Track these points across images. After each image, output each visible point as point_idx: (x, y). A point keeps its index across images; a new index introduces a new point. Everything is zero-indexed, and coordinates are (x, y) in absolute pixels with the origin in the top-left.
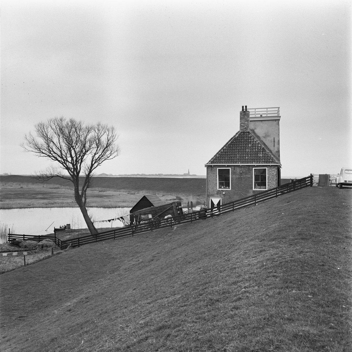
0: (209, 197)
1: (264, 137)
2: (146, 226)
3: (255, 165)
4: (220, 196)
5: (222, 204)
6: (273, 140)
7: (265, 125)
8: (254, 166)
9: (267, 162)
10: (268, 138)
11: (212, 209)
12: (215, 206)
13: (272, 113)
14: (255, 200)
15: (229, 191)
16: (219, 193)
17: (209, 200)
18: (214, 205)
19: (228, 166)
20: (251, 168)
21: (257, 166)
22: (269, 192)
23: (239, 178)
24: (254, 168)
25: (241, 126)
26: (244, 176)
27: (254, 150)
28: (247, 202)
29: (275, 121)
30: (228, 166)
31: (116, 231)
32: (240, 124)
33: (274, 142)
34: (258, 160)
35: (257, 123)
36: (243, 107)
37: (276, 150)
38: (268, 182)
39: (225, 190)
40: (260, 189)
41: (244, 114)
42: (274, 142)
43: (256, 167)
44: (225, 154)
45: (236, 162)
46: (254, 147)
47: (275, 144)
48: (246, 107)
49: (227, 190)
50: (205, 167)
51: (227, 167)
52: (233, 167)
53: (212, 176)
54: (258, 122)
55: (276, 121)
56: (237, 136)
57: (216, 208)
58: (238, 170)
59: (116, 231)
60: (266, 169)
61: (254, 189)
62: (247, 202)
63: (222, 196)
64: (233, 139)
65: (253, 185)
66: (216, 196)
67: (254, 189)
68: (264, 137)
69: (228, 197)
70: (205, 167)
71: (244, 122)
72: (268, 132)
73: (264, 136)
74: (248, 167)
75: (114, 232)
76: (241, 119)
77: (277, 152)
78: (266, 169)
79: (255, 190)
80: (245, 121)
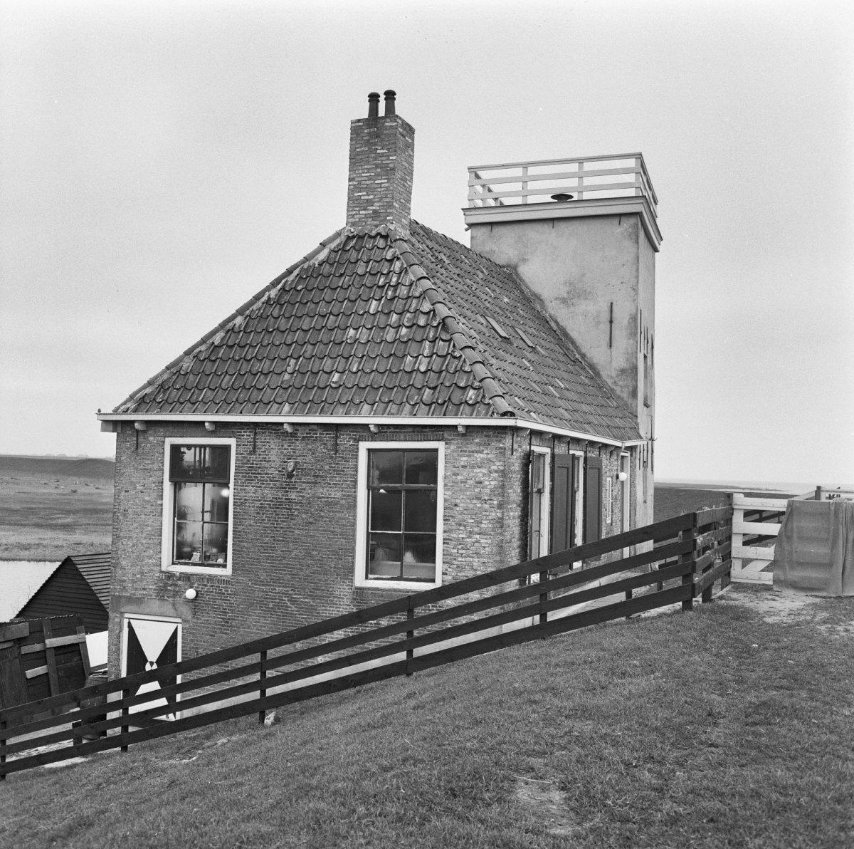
0: (122, 617)
1: (564, 301)
2: (638, 582)
3: (455, 427)
4: (172, 612)
5: (182, 657)
6: (605, 317)
7: (566, 241)
8: (362, 431)
9: (443, 406)
10: (583, 306)
11: (128, 687)
12: (148, 667)
13: (616, 185)
14: (408, 646)
15: (351, 570)
16: (168, 586)
17: (121, 630)
18: (146, 661)
19: (221, 428)
20: (345, 440)
21: (385, 431)
22: (450, 603)
23: (277, 505)
24: (364, 446)
25: (354, 203)
26: (308, 493)
27: (390, 335)
28: (321, 659)
29: (616, 221)
30: (221, 428)
31: (272, 653)
32: (351, 192)
33: (611, 322)
34: (395, 388)
35: (532, 232)
36: (374, 98)
37: (620, 362)
38: (445, 541)
39: (200, 577)
40: (400, 578)
41: (369, 134)
42: (611, 322)
43: (373, 437)
44: (229, 361)
45: (264, 405)
46: (395, 317)
47: (616, 333)
48: (390, 95)
49: (210, 578)
50: (103, 430)
51: (212, 434)
52: (247, 435)
53: (139, 487)
54: (538, 227)
55: (623, 219)
56: (322, 256)
57: (150, 677)
58: (274, 453)
59: (272, 653)
60: (436, 450)
61: (360, 580)
62: (321, 659)
63: (186, 611)
64: (296, 272)
65: (353, 550)
66: (155, 605)
67: (360, 580)
68: (564, 301)
69: (213, 617)
70: (103, 430)
71: (370, 178)
72: (583, 275)
73: (565, 296)
74: (328, 437)
75: (255, 658)
76: (355, 160)
77: (623, 371)
78: (436, 450)
79: (372, 584)
80: (377, 175)
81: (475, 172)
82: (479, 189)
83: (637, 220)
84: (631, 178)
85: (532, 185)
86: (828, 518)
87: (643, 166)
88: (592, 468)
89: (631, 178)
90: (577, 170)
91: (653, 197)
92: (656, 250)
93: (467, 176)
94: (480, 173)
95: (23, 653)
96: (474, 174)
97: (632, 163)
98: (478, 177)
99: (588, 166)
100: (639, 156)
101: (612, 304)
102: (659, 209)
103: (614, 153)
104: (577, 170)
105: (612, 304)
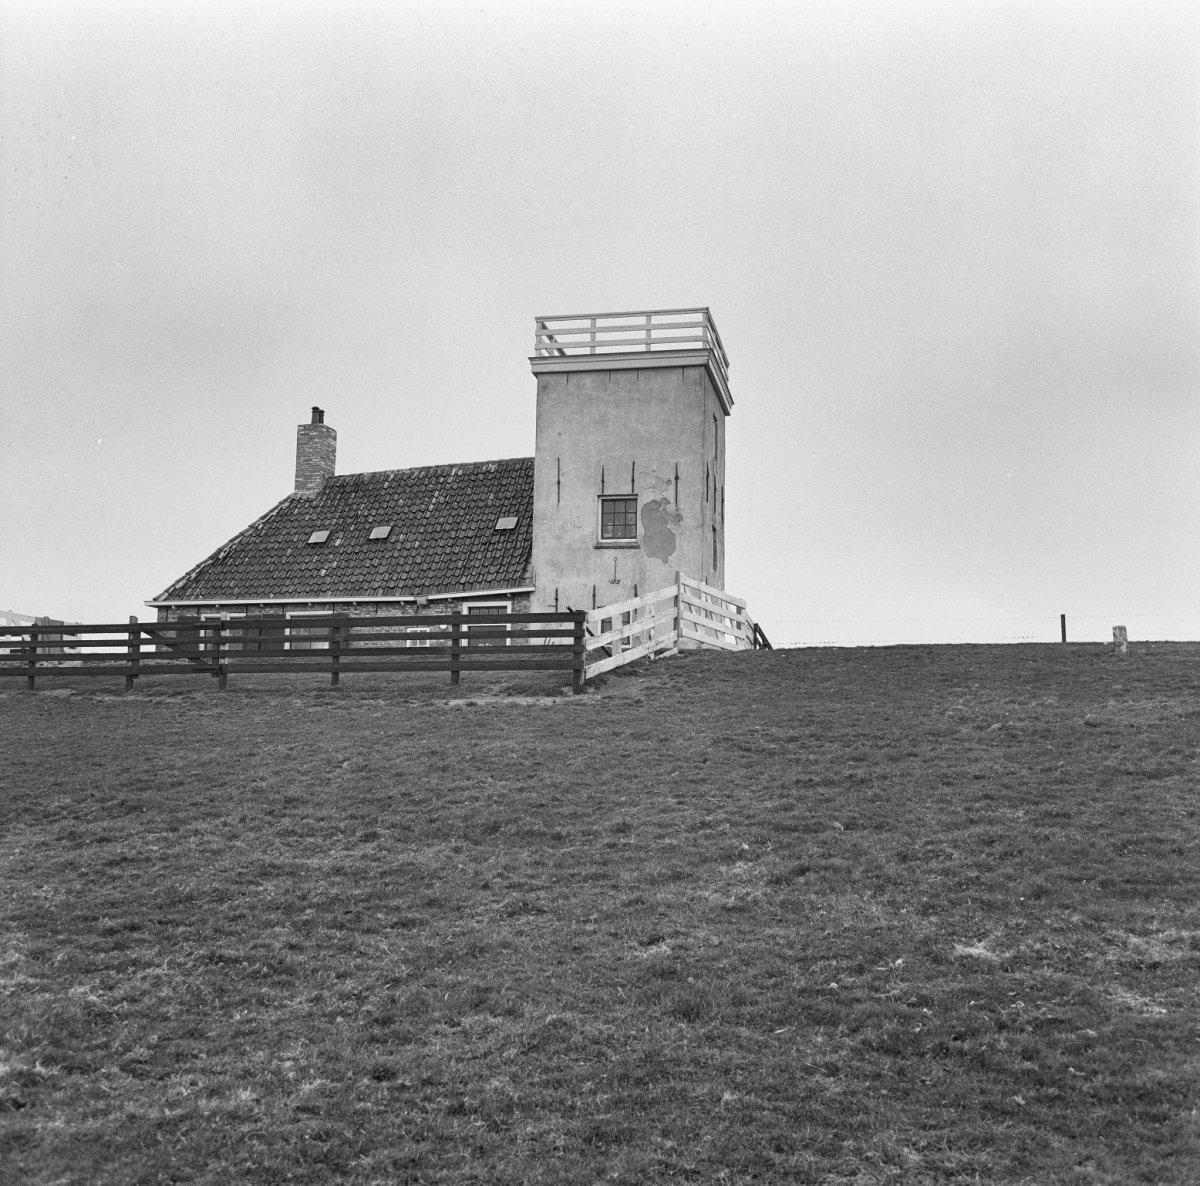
81: (542, 323)
82: (546, 340)
83: (704, 379)
84: (699, 332)
85: (600, 337)
86: (834, 695)
87: (709, 320)
88: (616, 559)
89: (699, 332)
90: (589, 326)
91: (724, 357)
92: (727, 413)
93: (534, 326)
94: (547, 324)
95: (371, 537)
96: (540, 324)
97: (699, 317)
98: (544, 327)
99: (655, 320)
100: (706, 311)
101: (1063, 617)
102: (730, 372)
103: (631, 310)
104: (589, 326)
105: (1063, 617)
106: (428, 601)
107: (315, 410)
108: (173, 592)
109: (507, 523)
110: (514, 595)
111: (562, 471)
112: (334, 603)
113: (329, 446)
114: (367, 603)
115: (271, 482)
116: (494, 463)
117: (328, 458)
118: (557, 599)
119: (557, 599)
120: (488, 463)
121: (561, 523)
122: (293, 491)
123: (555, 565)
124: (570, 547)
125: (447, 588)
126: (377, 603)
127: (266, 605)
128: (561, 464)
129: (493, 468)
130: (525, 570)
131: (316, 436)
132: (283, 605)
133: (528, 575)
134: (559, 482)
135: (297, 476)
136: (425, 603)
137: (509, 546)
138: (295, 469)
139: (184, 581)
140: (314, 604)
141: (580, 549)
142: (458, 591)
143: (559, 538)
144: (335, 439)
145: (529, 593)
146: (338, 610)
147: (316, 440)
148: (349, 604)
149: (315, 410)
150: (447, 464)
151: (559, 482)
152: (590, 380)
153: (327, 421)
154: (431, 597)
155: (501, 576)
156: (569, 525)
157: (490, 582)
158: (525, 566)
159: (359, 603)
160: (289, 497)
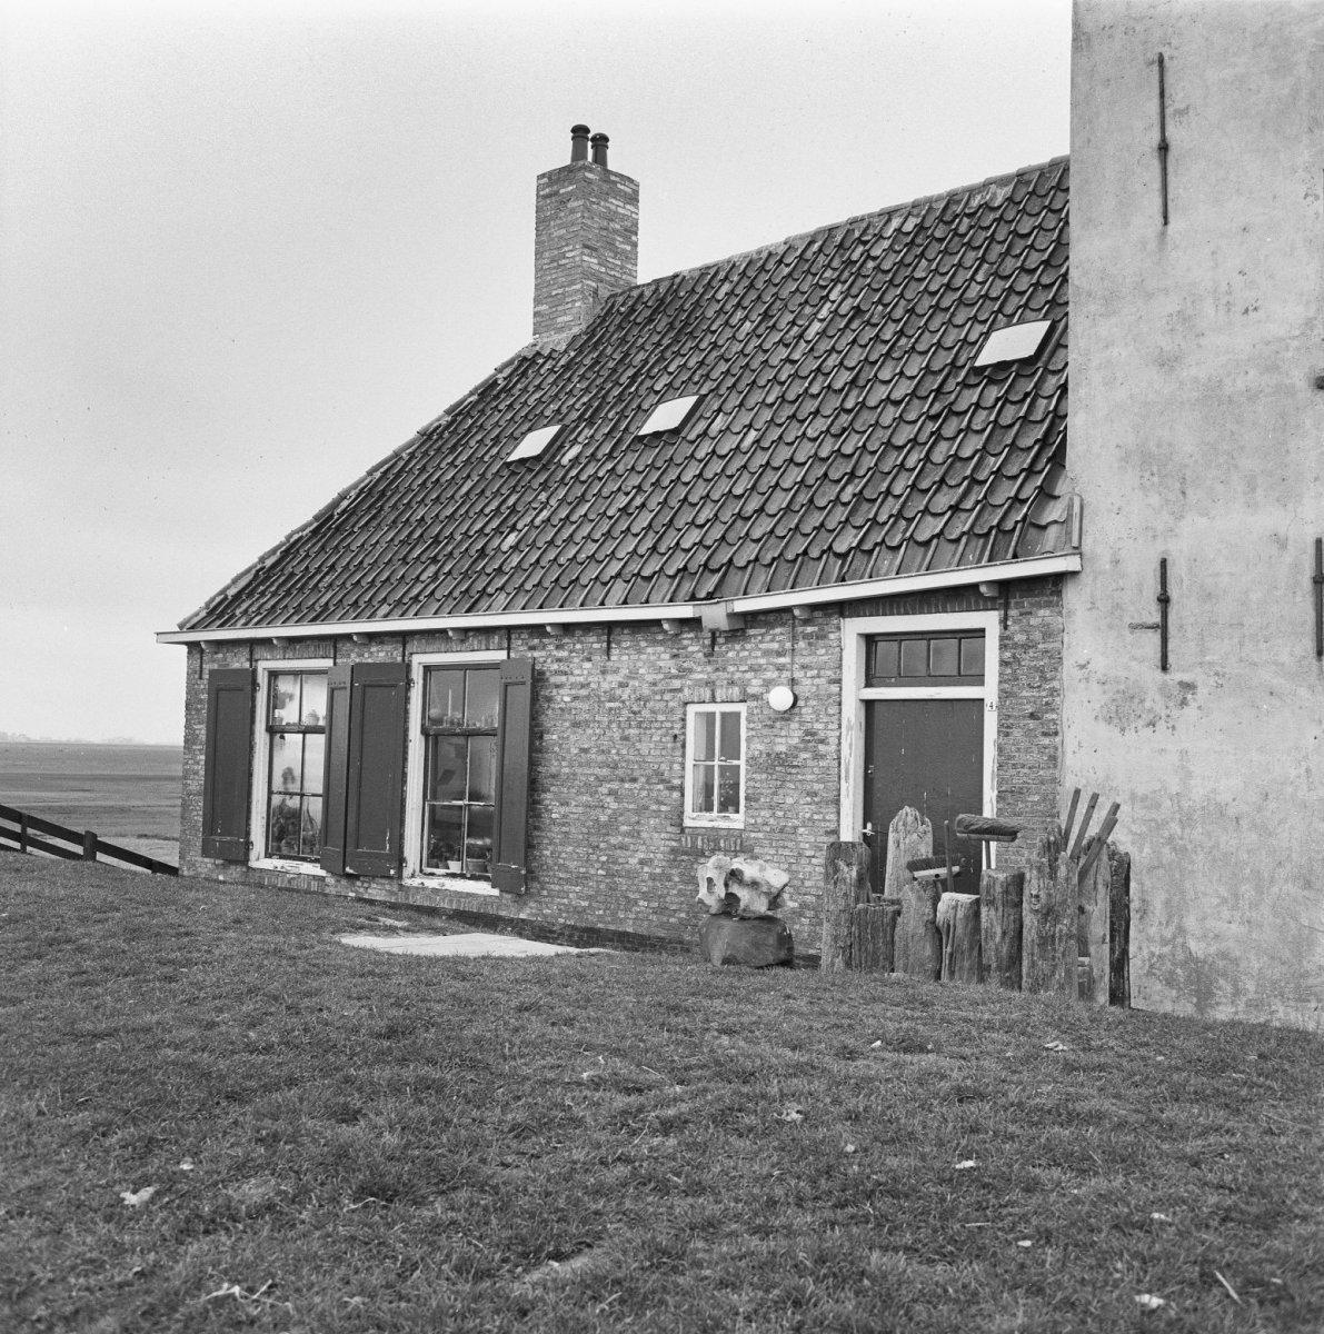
106: (732, 616)
107: (580, 132)
108: (221, 610)
109: (1013, 342)
110: (1006, 588)
111: (1176, 100)
112: (509, 630)
113: (612, 216)
114: (587, 627)
115: (484, 315)
116: (1002, 181)
117: (611, 245)
118: (1164, 601)
119: (1164, 601)
120: (986, 185)
121: (1171, 305)
122: (530, 339)
123: (1150, 463)
124: (1213, 397)
125: (795, 569)
126: (609, 628)
127: (372, 637)
128: (1170, 79)
129: (1002, 194)
130: (1046, 494)
131: (571, 194)
132: (404, 637)
133: (1054, 512)
134: (1164, 148)
135: (537, 301)
136: (724, 624)
137: (1010, 414)
138: (532, 282)
139: (249, 577)
140: (466, 631)
141: (1252, 396)
142: (822, 581)
143: (1167, 363)
144: (633, 199)
145: (1059, 579)
146: (520, 648)
147: (572, 204)
148: (537, 630)
149: (580, 132)
150: (876, 209)
151: (1164, 148)
152: (1311, 1026)
153: (614, 162)
154: (742, 606)
155: (963, 524)
156: (1208, 308)
157: (927, 544)
158: (1051, 478)
159: (567, 628)
160: (518, 356)
